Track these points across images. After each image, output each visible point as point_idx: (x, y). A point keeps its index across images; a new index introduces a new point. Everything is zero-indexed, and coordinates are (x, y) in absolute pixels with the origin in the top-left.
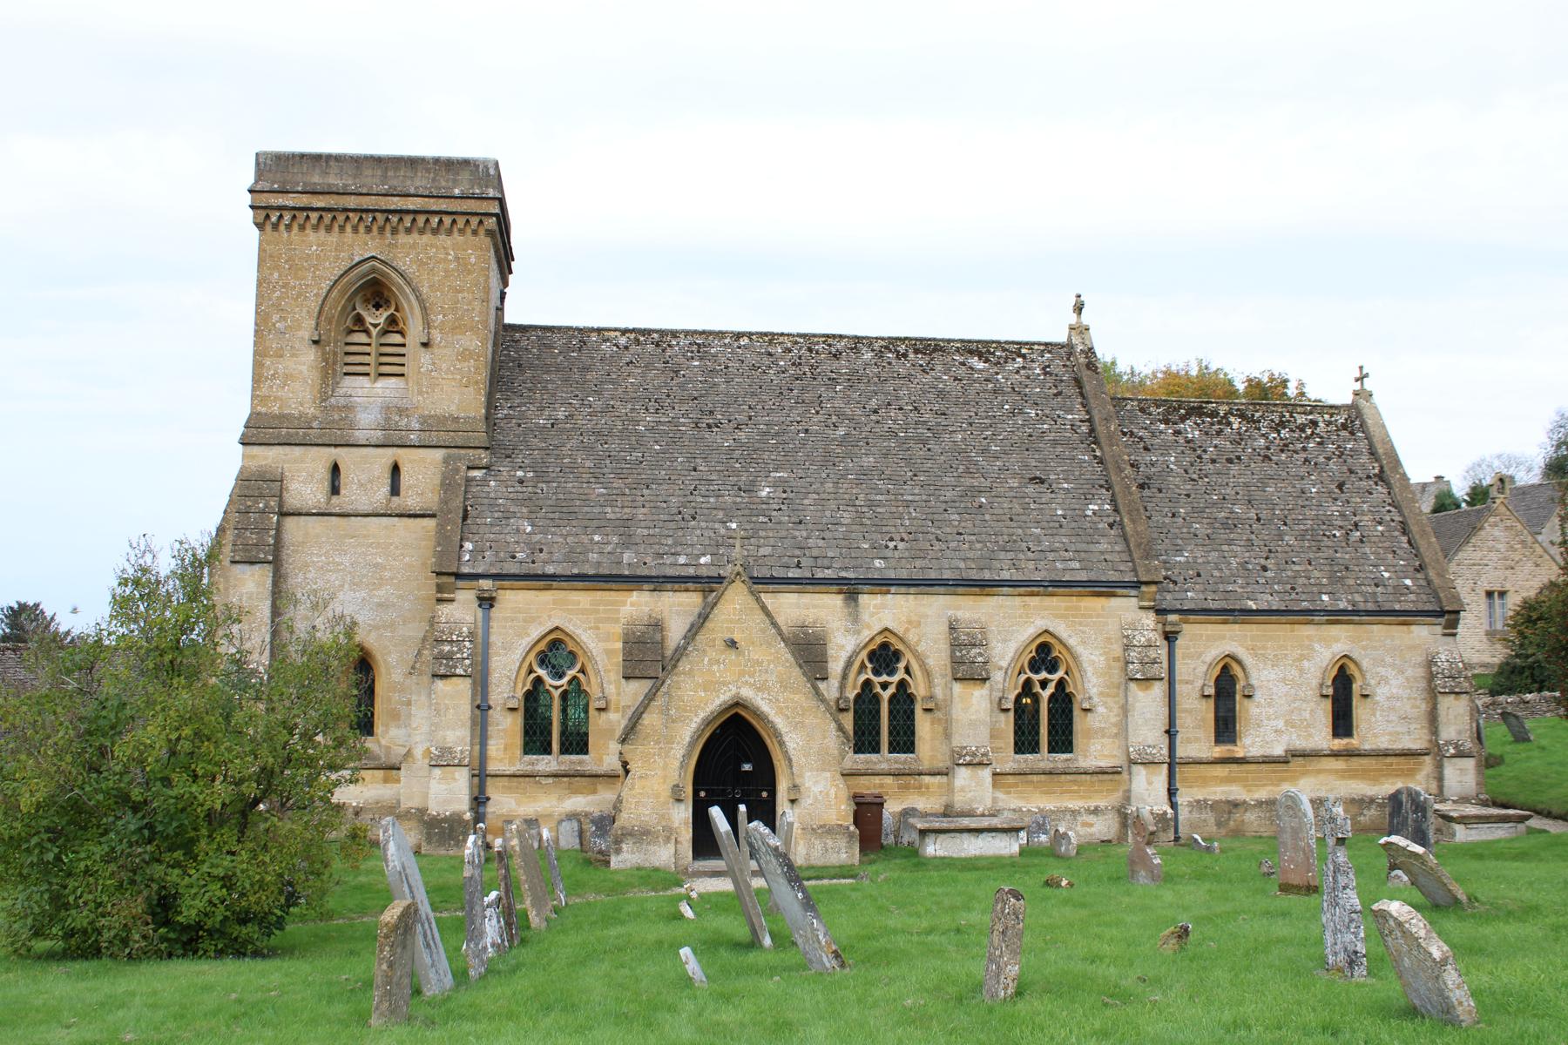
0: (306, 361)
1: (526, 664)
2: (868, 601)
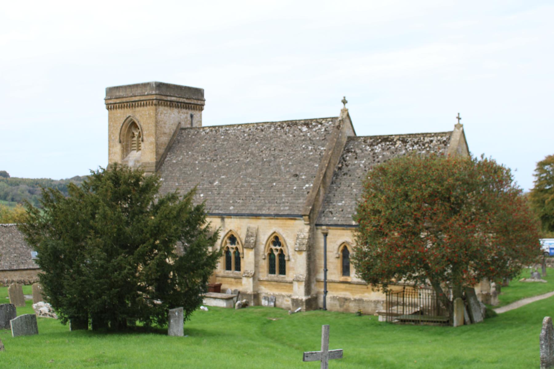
0: (118, 148)
1: (268, 243)
2: (227, 220)
